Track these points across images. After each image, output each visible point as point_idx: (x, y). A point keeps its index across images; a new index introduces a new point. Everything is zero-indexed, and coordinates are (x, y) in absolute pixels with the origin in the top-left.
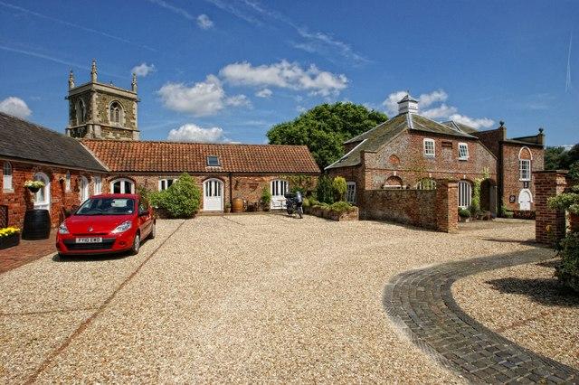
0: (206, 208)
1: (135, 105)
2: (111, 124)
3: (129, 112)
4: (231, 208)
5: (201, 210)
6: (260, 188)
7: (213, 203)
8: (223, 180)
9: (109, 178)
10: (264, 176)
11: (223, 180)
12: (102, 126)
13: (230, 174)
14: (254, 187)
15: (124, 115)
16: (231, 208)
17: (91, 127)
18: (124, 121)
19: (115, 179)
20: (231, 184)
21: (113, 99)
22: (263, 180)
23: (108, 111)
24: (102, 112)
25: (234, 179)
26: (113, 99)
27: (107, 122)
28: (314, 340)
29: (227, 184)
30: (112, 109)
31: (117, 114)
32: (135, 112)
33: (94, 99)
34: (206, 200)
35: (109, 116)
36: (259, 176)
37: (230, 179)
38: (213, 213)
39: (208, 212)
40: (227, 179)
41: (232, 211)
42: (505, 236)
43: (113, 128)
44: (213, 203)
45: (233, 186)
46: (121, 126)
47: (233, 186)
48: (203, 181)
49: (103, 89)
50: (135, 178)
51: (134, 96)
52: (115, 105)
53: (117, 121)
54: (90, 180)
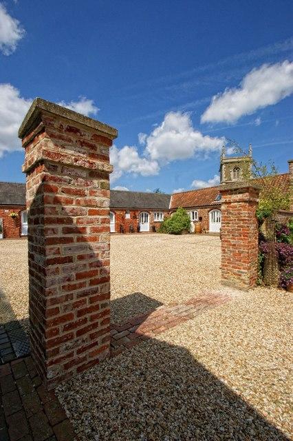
0: (211, 230)
7: (145, 227)
21: (234, 165)
24: (228, 175)
26: (234, 165)
27: (230, 179)
39: (212, 233)
48: (209, 212)
49: (229, 161)
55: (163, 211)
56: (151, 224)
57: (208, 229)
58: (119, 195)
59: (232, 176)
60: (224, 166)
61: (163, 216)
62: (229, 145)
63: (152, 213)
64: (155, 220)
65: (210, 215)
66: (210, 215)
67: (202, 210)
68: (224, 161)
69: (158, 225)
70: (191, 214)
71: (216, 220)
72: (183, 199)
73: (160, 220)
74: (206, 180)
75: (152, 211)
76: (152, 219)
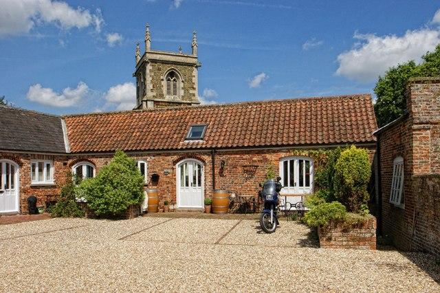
0: (180, 204)
1: (195, 72)
2: (167, 98)
3: (189, 80)
4: (211, 208)
5: (171, 207)
6: (260, 172)
7: (190, 197)
8: (203, 161)
9: (70, 161)
10: (268, 152)
11: (203, 161)
12: (155, 102)
13: (213, 151)
14: (250, 171)
15: (182, 85)
16: (211, 208)
17: (145, 103)
18: (182, 92)
19: (76, 162)
20: (213, 169)
21: (168, 68)
22: (266, 160)
23: (164, 83)
24: (157, 86)
25: (218, 159)
26: (168, 68)
27: (162, 96)
28: (433, 100)
29: (209, 167)
30: (169, 80)
31: (175, 86)
32: (195, 80)
33: (148, 71)
34: (181, 191)
35: (165, 89)
36: (259, 153)
37: (213, 159)
38: (189, 214)
39: (183, 210)
40: (208, 159)
41: (212, 211)
42: (151, 55)
43: (169, 103)
44: (190, 197)
45: (217, 171)
46: (178, 99)
47: (217, 171)
48: (175, 162)
49: (158, 57)
50: (95, 160)
51: (194, 61)
52: (172, 74)
53: (175, 93)
54: (21, 165)
55: (53, 158)
56: (23, 191)
57: (174, 202)
58: (44, 118)
59: (165, 89)
60: (149, 67)
61: (52, 170)
62: (108, 29)
63: (27, 164)
64: (34, 182)
65: (178, 170)
66: (178, 170)
67: (156, 158)
68: (149, 56)
69: (40, 195)
70: (281, 164)
71: (191, 180)
72: (100, 130)
73: (44, 182)
74: (58, 91)
75: (27, 157)
76: (25, 179)
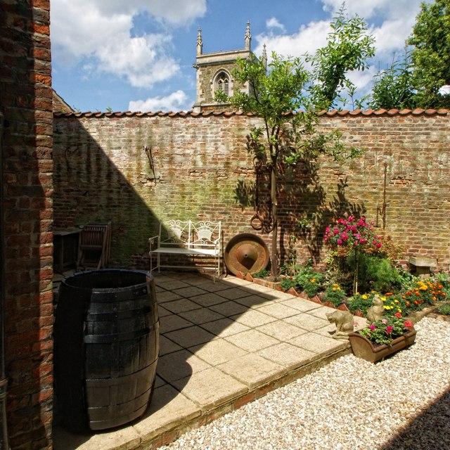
26: (217, 69)
